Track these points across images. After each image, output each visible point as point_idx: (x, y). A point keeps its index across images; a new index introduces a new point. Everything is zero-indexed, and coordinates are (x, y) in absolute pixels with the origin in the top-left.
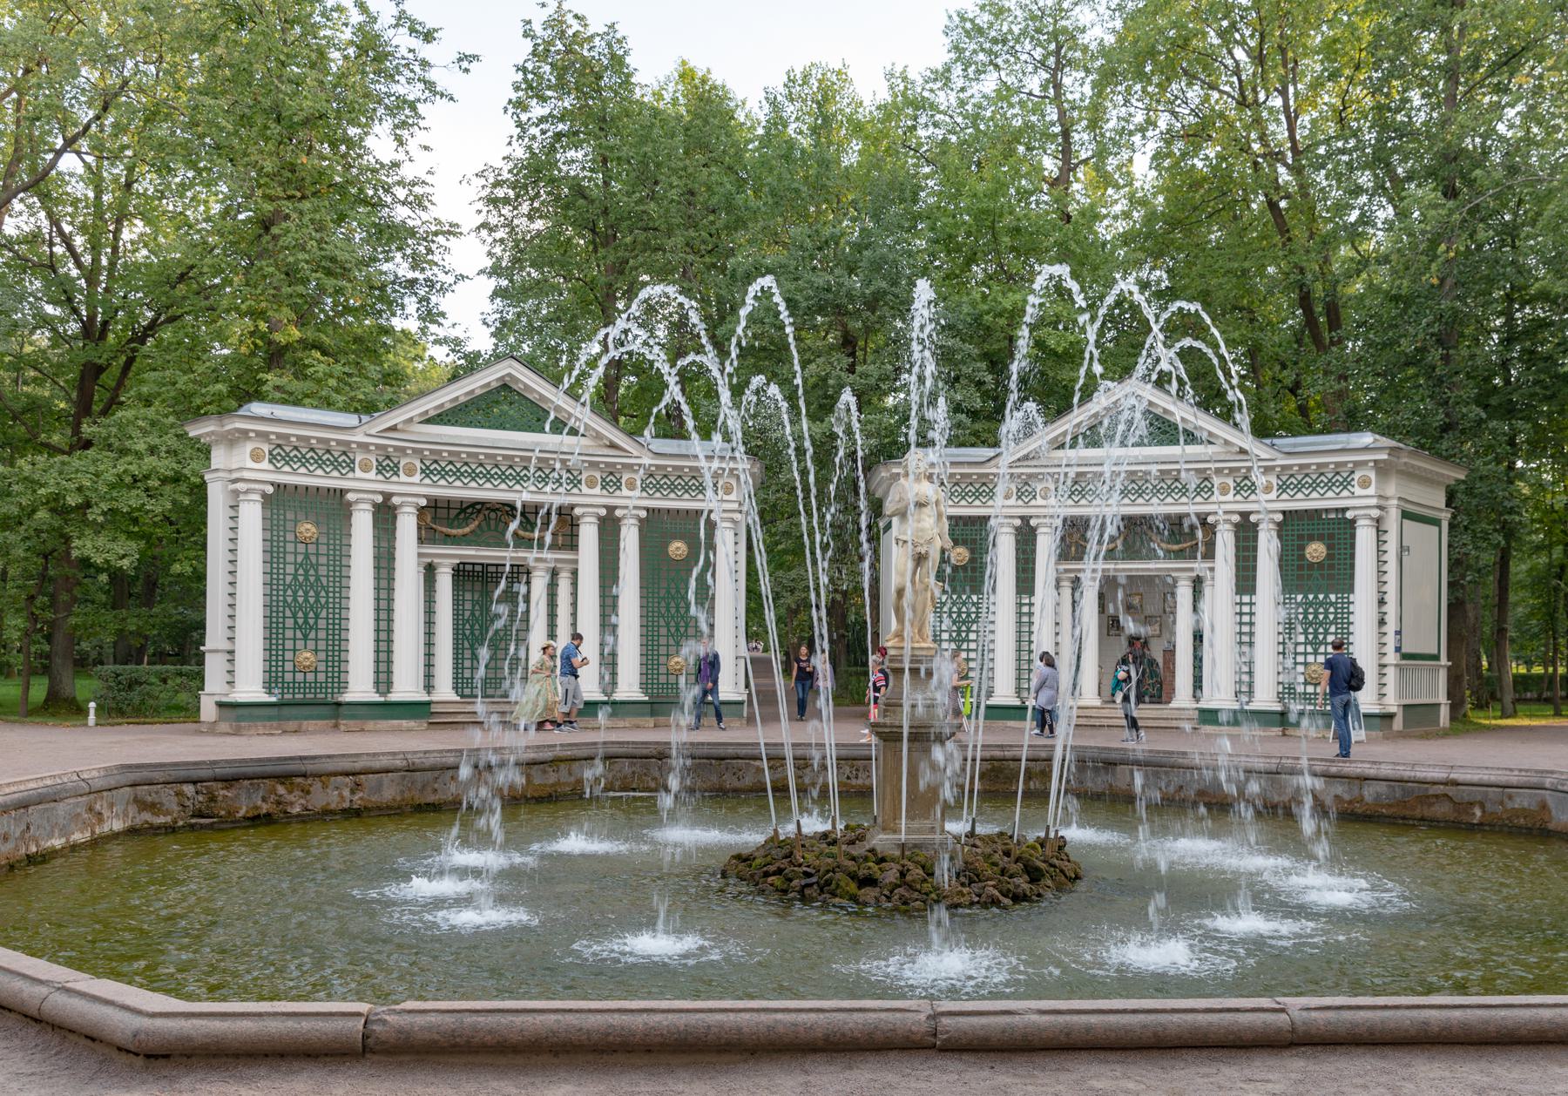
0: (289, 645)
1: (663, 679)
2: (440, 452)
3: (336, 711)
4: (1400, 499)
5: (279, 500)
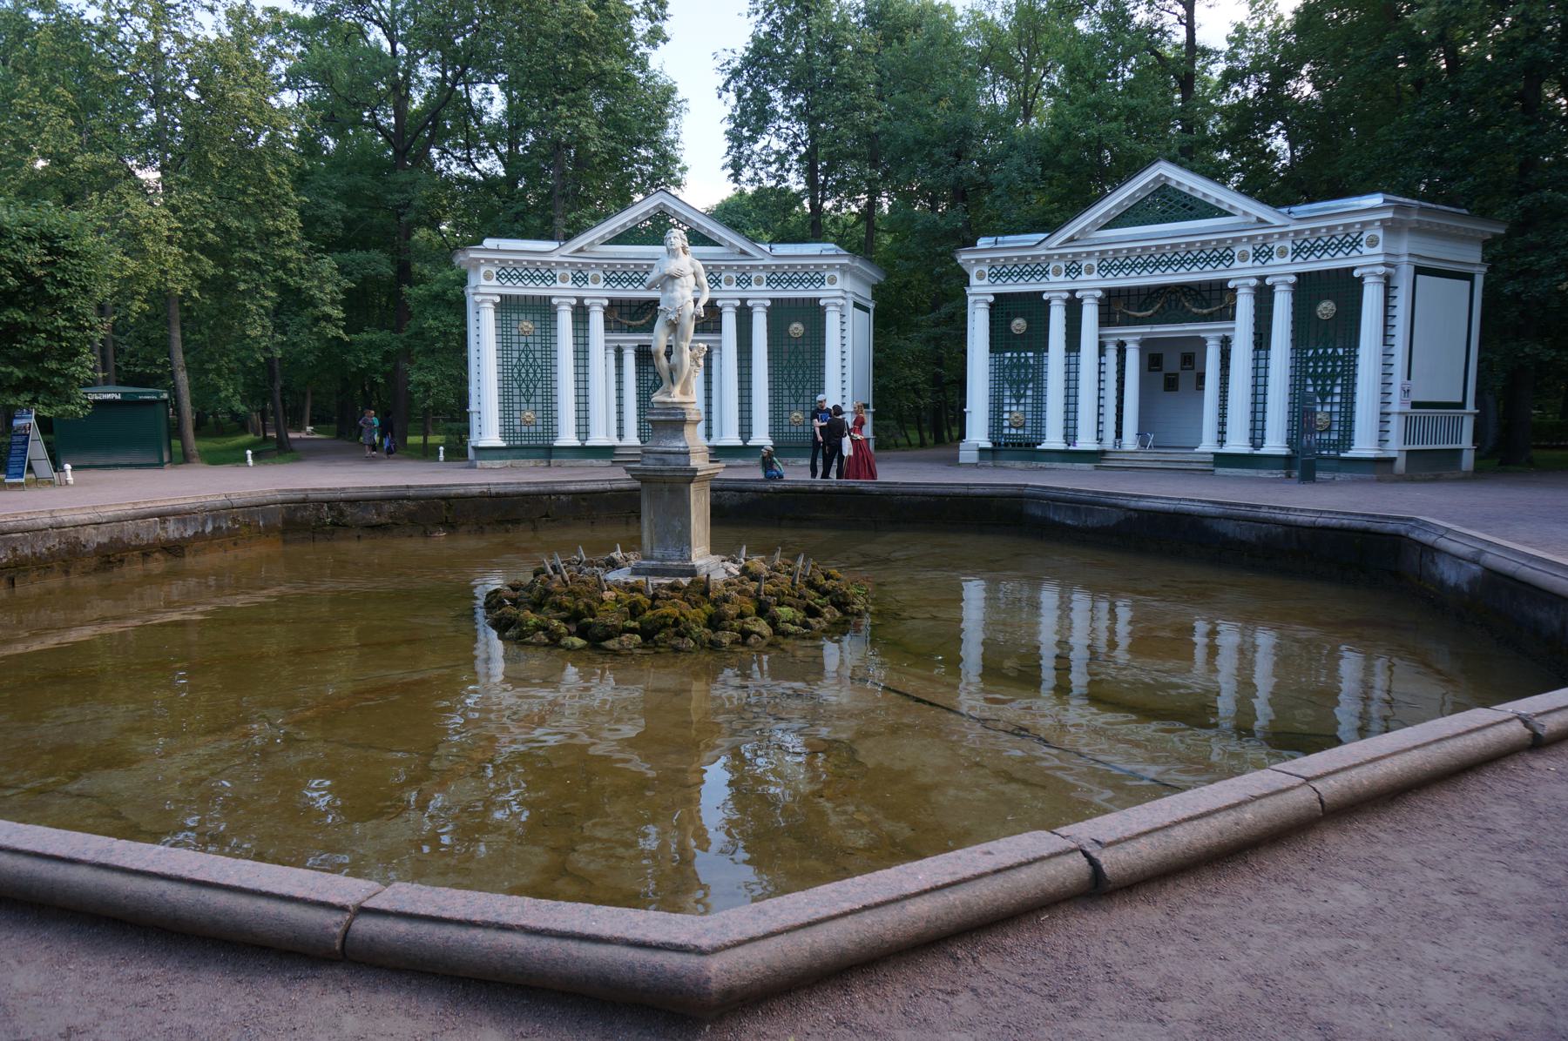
0: (517, 407)
1: (786, 429)
2: (628, 265)
3: (549, 452)
4: (1410, 255)
5: (507, 307)
